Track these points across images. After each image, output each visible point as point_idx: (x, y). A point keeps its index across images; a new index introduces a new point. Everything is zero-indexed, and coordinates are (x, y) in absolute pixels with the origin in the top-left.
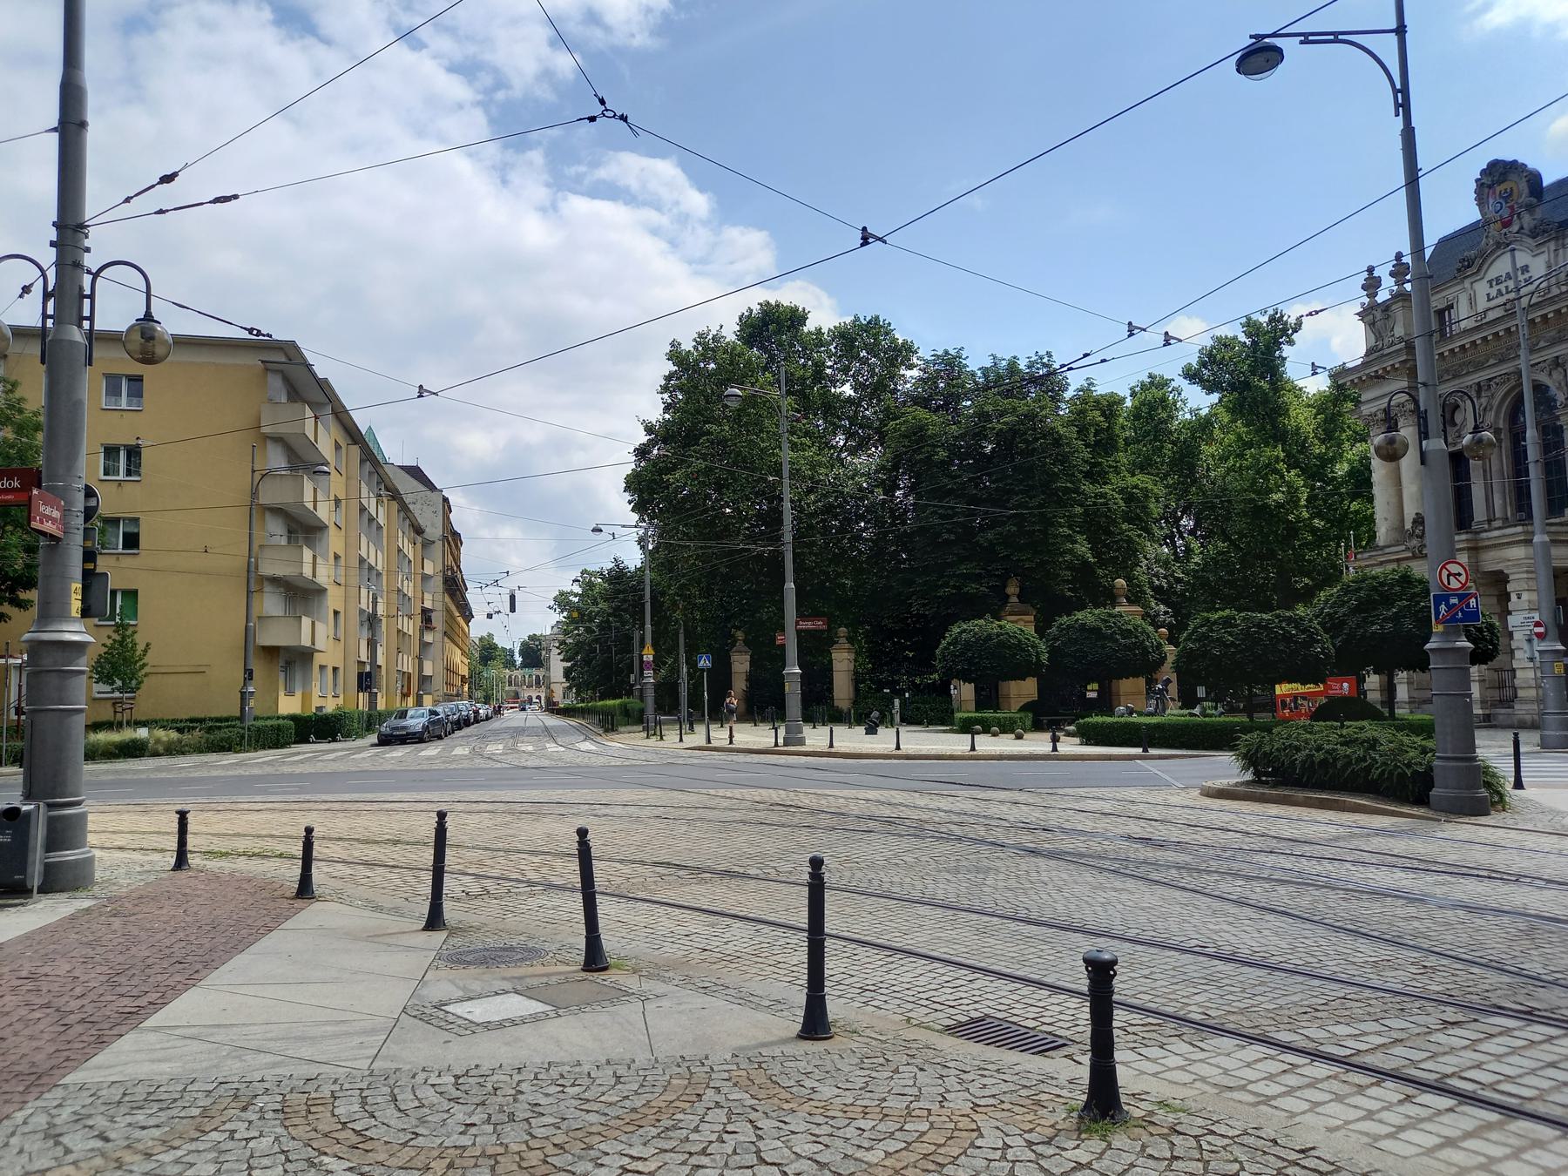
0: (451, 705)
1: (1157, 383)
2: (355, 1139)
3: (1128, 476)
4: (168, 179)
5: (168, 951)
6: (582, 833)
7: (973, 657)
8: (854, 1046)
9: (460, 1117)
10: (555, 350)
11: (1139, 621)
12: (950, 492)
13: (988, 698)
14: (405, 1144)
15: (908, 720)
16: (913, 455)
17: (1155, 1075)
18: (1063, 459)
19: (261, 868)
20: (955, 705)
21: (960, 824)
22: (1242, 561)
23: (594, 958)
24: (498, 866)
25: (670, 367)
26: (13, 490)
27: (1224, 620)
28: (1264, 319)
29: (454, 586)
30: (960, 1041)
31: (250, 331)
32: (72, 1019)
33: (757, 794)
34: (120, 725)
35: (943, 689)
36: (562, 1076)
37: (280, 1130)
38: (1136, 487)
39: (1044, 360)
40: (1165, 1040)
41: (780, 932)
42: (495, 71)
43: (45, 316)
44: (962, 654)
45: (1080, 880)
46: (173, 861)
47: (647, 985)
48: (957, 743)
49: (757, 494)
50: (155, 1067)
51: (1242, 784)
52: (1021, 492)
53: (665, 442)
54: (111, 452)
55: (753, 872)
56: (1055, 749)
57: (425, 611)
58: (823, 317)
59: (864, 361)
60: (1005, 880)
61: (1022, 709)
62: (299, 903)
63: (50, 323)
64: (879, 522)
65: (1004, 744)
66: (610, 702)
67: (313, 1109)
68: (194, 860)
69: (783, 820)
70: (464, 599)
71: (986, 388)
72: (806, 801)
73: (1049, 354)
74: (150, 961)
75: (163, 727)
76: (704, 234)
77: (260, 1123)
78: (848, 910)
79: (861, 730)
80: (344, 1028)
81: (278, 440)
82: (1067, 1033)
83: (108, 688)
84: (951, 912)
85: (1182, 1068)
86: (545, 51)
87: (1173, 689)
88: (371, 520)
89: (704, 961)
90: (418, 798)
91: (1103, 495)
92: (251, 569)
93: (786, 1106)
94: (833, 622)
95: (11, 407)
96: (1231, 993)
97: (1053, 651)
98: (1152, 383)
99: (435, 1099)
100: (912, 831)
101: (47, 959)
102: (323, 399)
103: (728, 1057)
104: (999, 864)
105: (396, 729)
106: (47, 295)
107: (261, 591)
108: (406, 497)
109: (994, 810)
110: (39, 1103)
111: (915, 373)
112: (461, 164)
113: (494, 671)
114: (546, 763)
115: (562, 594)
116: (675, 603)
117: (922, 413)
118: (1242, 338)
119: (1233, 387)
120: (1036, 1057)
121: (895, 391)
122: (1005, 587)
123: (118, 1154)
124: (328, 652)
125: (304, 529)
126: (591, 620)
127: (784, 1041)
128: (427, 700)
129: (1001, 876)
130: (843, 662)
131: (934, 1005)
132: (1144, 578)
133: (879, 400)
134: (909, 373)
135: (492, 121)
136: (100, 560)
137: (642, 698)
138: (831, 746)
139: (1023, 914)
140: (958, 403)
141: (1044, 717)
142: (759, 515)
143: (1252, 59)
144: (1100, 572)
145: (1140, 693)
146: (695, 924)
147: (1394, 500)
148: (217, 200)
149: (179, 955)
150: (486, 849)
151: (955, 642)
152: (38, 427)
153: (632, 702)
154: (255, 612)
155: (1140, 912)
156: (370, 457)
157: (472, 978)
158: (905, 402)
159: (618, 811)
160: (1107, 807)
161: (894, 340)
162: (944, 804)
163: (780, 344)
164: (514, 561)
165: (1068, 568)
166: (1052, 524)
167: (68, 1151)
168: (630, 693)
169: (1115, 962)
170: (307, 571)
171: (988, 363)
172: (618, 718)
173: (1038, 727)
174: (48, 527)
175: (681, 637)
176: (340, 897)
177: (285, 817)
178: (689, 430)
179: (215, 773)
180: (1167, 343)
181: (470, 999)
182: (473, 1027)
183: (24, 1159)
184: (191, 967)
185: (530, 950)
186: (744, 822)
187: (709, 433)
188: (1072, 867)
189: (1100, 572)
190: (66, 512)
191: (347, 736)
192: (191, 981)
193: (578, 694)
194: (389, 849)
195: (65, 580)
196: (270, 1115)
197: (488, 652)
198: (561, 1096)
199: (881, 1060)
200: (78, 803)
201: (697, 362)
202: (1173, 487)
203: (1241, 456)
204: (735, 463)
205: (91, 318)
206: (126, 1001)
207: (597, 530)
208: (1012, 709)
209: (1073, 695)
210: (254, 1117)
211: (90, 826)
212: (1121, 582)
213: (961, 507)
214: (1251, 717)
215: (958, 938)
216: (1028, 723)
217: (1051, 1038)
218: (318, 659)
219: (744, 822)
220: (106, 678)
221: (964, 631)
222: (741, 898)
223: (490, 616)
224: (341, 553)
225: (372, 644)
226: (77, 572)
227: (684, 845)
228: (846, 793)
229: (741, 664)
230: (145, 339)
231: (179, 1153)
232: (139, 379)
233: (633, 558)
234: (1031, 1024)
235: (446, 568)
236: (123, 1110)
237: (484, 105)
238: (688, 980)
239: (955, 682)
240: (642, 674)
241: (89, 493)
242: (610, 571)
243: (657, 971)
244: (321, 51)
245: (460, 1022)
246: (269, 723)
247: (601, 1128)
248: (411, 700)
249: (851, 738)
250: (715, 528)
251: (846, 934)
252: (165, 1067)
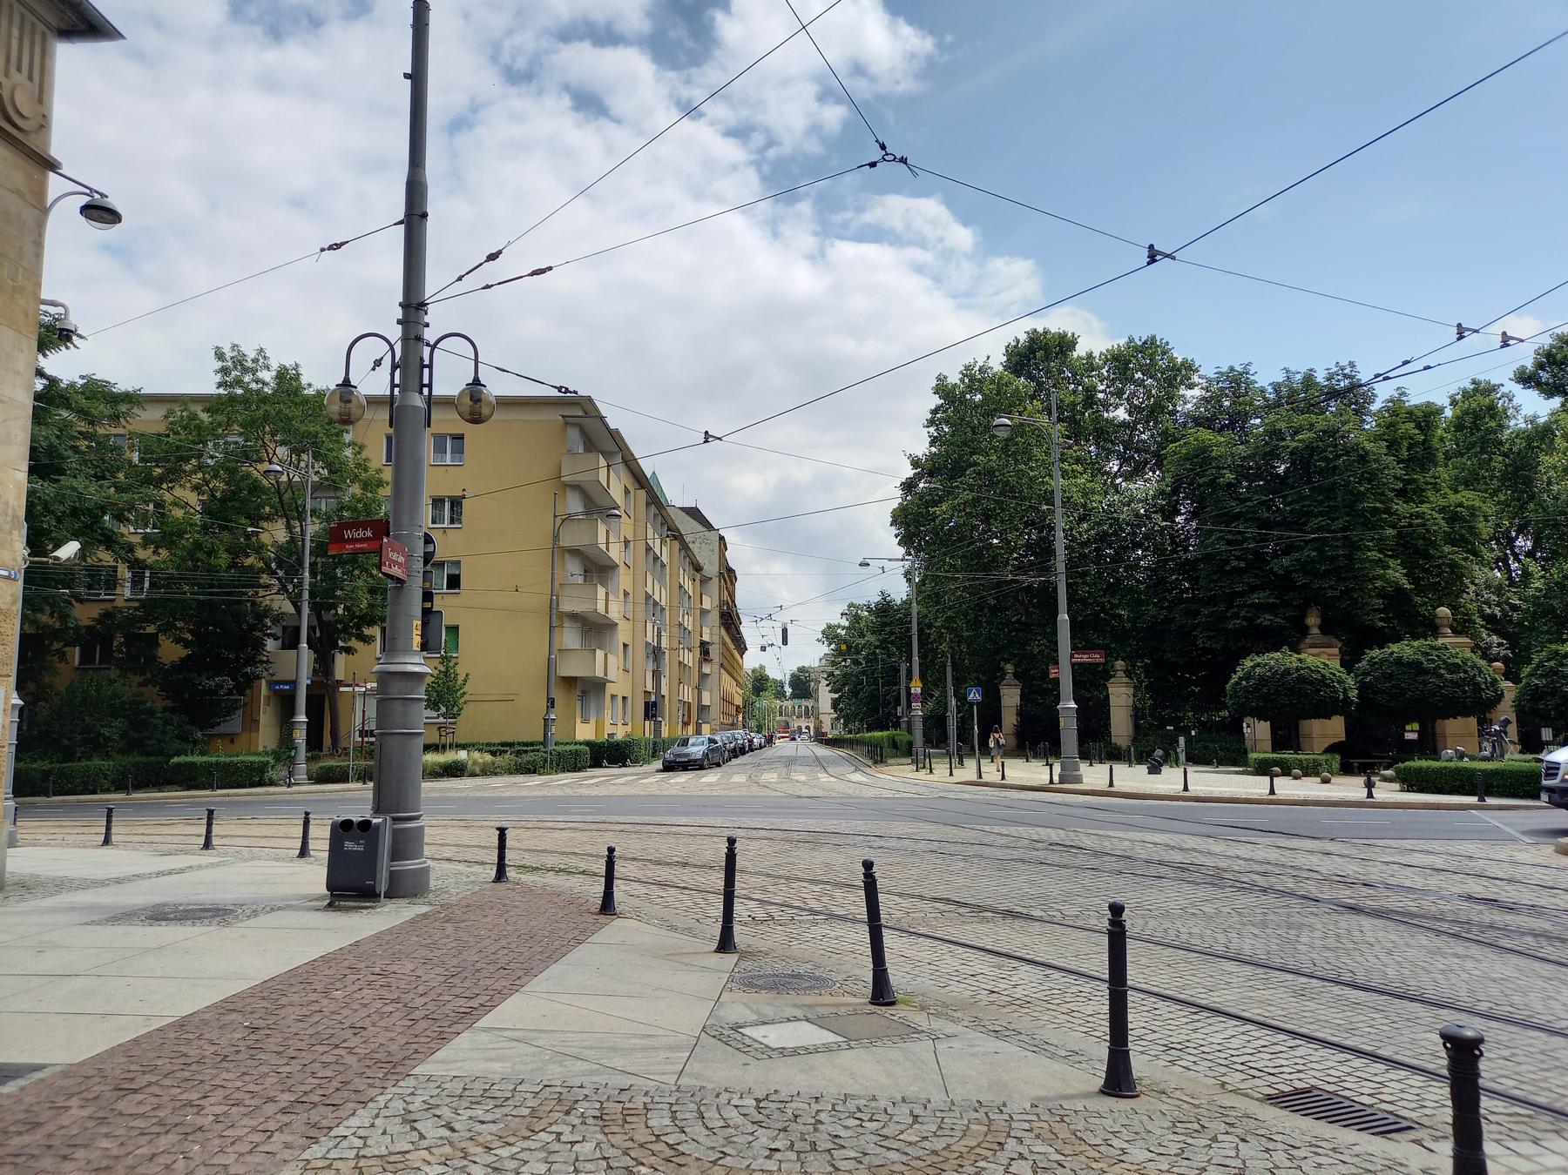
0: (728, 734)
2: (669, 1153)
3: (1446, 492)
4: (492, 257)
6: (868, 865)
8: (1164, 1108)
10: (825, 392)
11: (1468, 654)
12: (1238, 517)
13: (1286, 738)
14: (714, 1162)
15: (1193, 759)
16: (1196, 481)
18: (1372, 477)
19: (568, 884)
20: (1248, 744)
21: (1264, 874)
23: (882, 993)
24: (781, 893)
25: (937, 401)
29: (730, 620)
30: (1285, 1112)
32: (417, 1015)
33: (1035, 833)
35: (1234, 727)
36: (859, 1110)
37: (600, 1137)
38: (1461, 505)
40: (1539, 1135)
42: (767, 130)
43: (393, 386)
44: (1256, 689)
45: (1412, 942)
46: (493, 873)
47: (937, 1024)
48: (1257, 786)
49: (1026, 525)
52: (1321, 514)
53: (931, 474)
54: (438, 502)
56: (1370, 795)
57: (703, 644)
59: (1140, 383)
60: (1323, 939)
64: (1159, 550)
65: (1309, 788)
67: (629, 1119)
68: (511, 873)
69: (1064, 861)
70: (739, 632)
71: (1277, 404)
72: (1087, 842)
73: (1352, 365)
74: (478, 966)
75: (480, 750)
77: (584, 1127)
79: (1143, 769)
80: (650, 1042)
81: (576, 487)
82: (1413, 1115)
86: (813, 106)
87: (1513, 730)
88: (656, 558)
89: (992, 1003)
92: (553, 606)
94: (1110, 654)
95: (358, 465)
97: (1363, 688)
98: (1476, 390)
99: (740, 1120)
100: (1209, 879)
101: (396, 958)
104: (1312, 919)
105: (678, 756)
106: (394, 367)
108: (682, 533)
109: (1302, 860)
110: (395, 1090)
111: (1197, 392)
112: (737, 221)
113: (766, 702)
115: (829, 627)
117: (1205, 435)
120: (1378, 1139)
122: (1304, 616)
123: (463, 1145)
124: (619, 684)
125: (598, 569)
126: (858, 653)
127: (1086, 1095)
128: (706, 728)
129: (1317, 934)
130: (1120, 697)
131: (1253, 1073)
132: (1473, 607)
133: (1156, 423)
134: (1189, 393)
135: (765, 179)
136: (436, 599)
139: (1347, 977)
140: (1245, 422)
141: (1355, 757)
142: (1028, 546)
144: (1418, 599)
145: (1471, 735)
146: (980, 963)
147: (48, 61)
148: (534, 273)
149: (504, 960)
150: (768, 875)
151: (1248, 677)
152: (380, 484)
153: (901, 735)
154: (556, 647)
155: (1491, 984)
156: (655, 501)
157: (765, 1002)
158: (1185, 424)
159: (893, 843)
160: (1439, 862)
161: (1172, 360)
162: (1243, 851)
163: (1048, 371)
164: (785, 597)
165: (1378, 596)
166: (1359, 549)
167: (422, 1137)
168: (897, 725)
169: (1481, 1041)
170: (601, 608)
171: (1280, 378)
172: (887, 751)
173: (1347, 770)
174: (395, 571)
175: (949, 669)
176: (638, 915)
177: (585, 837)
178: (956, 462)
179: (524, 793)
182: (768, 1052)
183: (388, 1139)
184: (514, 975)
185: (817, 979)
186: (1023, 861)
187: (976, 464)
188: (1402, 928)
190: (409, 557)
191: (636, 762)
192: (514, 988)
193: (845, 725)
194: (679, 871)
195: (411, 618)
196: (590, 1121)
197: (760, 683)
198: (860, 1130)
199: (1196, 1126)
201: (963, 394)
204: (1002, 494)
205: (430, 386)
206: (461, 1002)
207: (864, 564)
208: (1314, 751)
210: (577, 1121)
213: (1252, 531)
216: (1336, 766)
218: (610, 689)
219: (1023, 861)
220: (433, 705)
221: (1258, 665)
222: (1026, 940)
223: (763, 649)
225: (657, 675)
226: (418, 612)
227: (962, 881)
229: (1011, 697)
231: (515, 1150)
233: (899, 591)
235: (722, 603)
236: (465, 1104)
237: (757, 165)
238: (977, 1023)
239: (1248, 720)
240: (909, 706)
241: (428, 540)
242: (877, 604)
243: (945, 1010)
244: (611, 130)
245: (757, 1045)
246: (568, 748)
248: (691, 729)
249: (1132, 777)
250: (983, 560)
251: (1144, 986)
252: (496, 1066)
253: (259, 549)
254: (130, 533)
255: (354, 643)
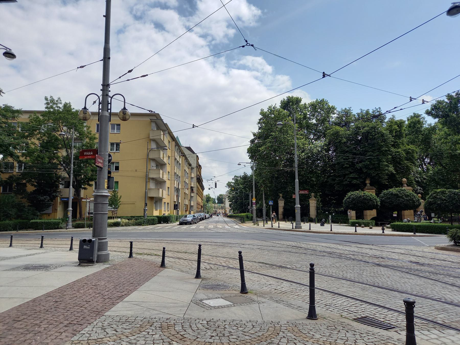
1: (416, 116)
2: (181, 337)
3: (405, 146)
4: (130, 71)
5: (129, 280)
6: (240, 253)
7: (355, 203)
8: (325, 322)
9: (209, 333)
10: (228, 113)
11: (411, 192)
12: (347, 152)
13: (360, 216)
14: (195, 340)
15: (333, 222)
16: (335, 141)
17: (427, 340)
18: (385, 141)
19: (151, 258)
20: (349, 217)
21: (353, 255)
22: (447, 173)
23: (244, 290)
24: (214, 261)
25: (261, 117)
26: (91, 155)
27: (442, 192)
28: (454, 94)
29: (199, 180)
30: (359, 324)
31: (150, 111)
32: (106, 297)
33: (290, 243)
34: (114, 218)
37: (161, 333)
38: (410, 149)
39: (379, 110)
41: (298, 285)
42: (212, 36)
43: (99, 109)
44: (352, 202)
47: (260, 299)
48: (351, 229)
49: (286, 153)
50: (127, 312)
51: (450, 245)
53: (259, 138)
54: (112, 144)
55: (289, 266)
56: (383, 232)
57: (191, 187)
58: (306, 100)
59: (320, 113)
61: (371, 219)
62: (161, 269)
63: (100, 111)
64: (324, 161)
65: (366, 230)
66: (243, 214)
68: (134, 255)
69: (296, 251)
70: (202, 184)
72: (303, 246)
73: (380, 108)
74: (124, 283)
76: (270, 77)
77: (156, 330)
78: (319, 280)
79: (319, 224)
80: (176, 305)
81: (154, 140)
82: (395, 324)
83: (111, 208)
84: (353, 283)
85: (437, 339)
86: (225, 29)
88: (178, 162)
89: (276, 293)
90: (191, 240)
91: (398, 152)
92: (147, 176)
93: (305, 339)
95: (88, 133)
96: (452, 315)
97: (382, 202)
98: (414, 116)
99: (202, 328)
100: (338, 256)
101: (99, 280)
102: (166, 129)
103: (286, 322)
104: (367, 268)
106: (100, 103)
107: (149, 182)
108: (186, 154)
109: (364, 251)
111: (336, 115)
113: (210, 204)
114: (226, 231)
115: (229, 182)
116: (261, 185)
117: (338, 128)
118: (446, 100)
119: (443, 117)
121: (329, 121)
123: (120, 336)
124: (166, 199)
125: (160, 165)
126: (237, 190)
127: (303, 319)
128: (192, 212)
130: (313, 204)
131: (350, 312)
132: (413, 178)
134: (333, 116)
135: (211, 50)
136: (112, 173)
137: (252, 213)
138: (310, 229)
139: (376, 284)
141: (379, 221)
142: (287, 159)
143: (451, 11)
144: (397, 176)
146: (272, 281)
149: (132, 281)
151: (349, 198)
153: (249, 214)
154: (148, 188)
155: (417, 286)
156: (178, 145)
157: (210, 293)
158: (332, 124)
159: (247, 246)
160: (403, 251)
161: (329, 106)
162: (348, 248)
164: (216, 174)
166: (381, 162)
167: (107, 334)
168: (248, 212)
169: (415, 302)
171: (359, 112)
172: (245, 219)
173: (377, 225)
174: (100, 165)
175: (263, 195)
176: (172, 267)
178: (266, 135)
180: (423, 103)
181: (209, 299)
182: (211, 307)
184: (135, 285)
186: (285, 251)
187: (272, 135)
188: (392, 270)
189: (397, 176)
190: (104, 161)
191: (171, 222)
192: (135, 289)
193: (233, 211)
196: (158, 328)
197: (208, 199)
199: (334, 328)
200: (106, 239)
201: (268, 115)
202: (422, 149)
203: (446, 138)
205: (110, 109)
206: (119, 293)
209: (387, 215)
210: (154, 328)
211: (108, 245)
212: (404, 180)
213: (351, 156)
214: (452, 224)
215: (356, 291)
216: (374, 224)
217: (389, 325)
218: (164, 201)
219: (285, 251)
220: (110, 205)
223: (209, 189)
224: (170, 171)
225: (178, 196)
228: (315, 244)
229: (281, 204)
230: (124, 115)
232: (119, 125)
233: (249, 172)
234: (382, 320)
235: (197, 175)
237: (209, 46)
238: (271, 298)
239: (349, 210)
240: (252, 206)
241: (110, 156)
242: (243, 176)
243: (262, 295)
244: (166, 34)
245: (207, 306)
246: (151, 218)
247: (250, 341)
249: (316, 227)
250: (274, 164)
252: (130, 312)
253: (58, 158)
254: (18, 152)
255: (86, 186)
